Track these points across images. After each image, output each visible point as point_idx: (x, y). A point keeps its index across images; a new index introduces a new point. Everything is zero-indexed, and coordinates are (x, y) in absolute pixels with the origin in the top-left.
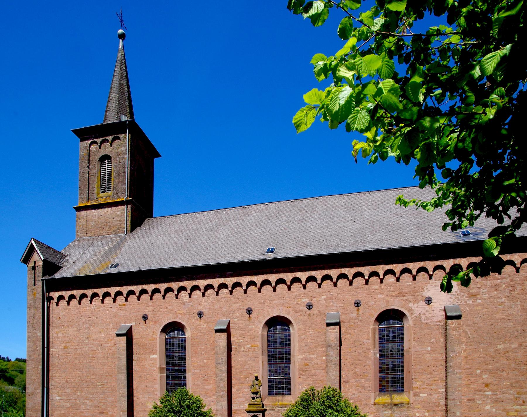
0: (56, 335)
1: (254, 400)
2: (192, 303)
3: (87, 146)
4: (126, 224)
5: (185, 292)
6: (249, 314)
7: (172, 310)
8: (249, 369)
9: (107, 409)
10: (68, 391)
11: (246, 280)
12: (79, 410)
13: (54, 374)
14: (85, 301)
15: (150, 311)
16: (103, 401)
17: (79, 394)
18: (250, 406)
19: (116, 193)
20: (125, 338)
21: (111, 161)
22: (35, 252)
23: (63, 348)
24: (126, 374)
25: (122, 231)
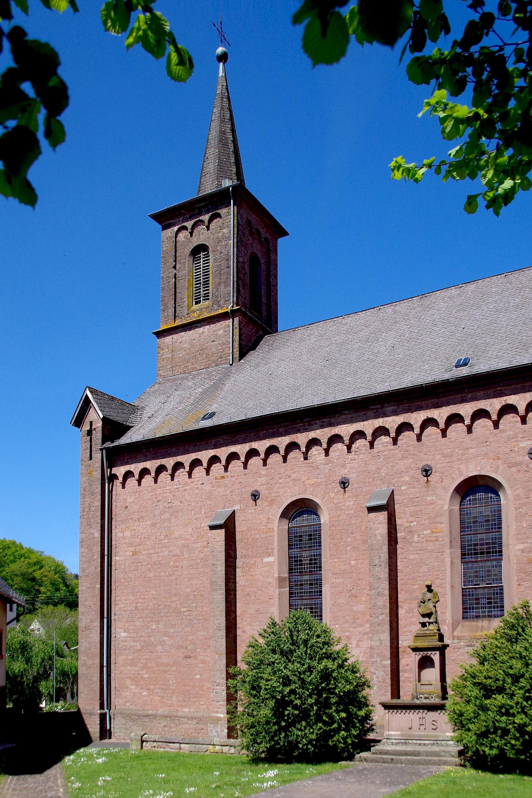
0: (121, 535)
1: (425, 628)
2: (330, 465)
3: (172, 235)
4: (231, 349)
5: (318, 448)
6: (427, 476)
7: (298, 480)
8: (428, 574)
9: (196, 651)
10: (138, 624)
11: (420, 418)
12: (154, 654)
13: (119, 596)
14: (164, 476)
15: (263, 485)
16: (190, 638)
17: (154, 627)
18: (418, 640)
19: (217, 302)
20: (222, 532)
21: (208, 252)
22: (91, 407)
23: (131, 554)
24: (224, 591)
25: (226, 359)
